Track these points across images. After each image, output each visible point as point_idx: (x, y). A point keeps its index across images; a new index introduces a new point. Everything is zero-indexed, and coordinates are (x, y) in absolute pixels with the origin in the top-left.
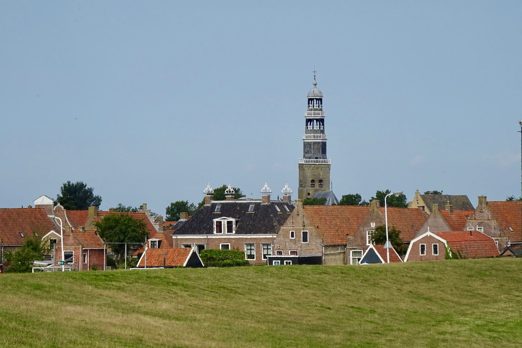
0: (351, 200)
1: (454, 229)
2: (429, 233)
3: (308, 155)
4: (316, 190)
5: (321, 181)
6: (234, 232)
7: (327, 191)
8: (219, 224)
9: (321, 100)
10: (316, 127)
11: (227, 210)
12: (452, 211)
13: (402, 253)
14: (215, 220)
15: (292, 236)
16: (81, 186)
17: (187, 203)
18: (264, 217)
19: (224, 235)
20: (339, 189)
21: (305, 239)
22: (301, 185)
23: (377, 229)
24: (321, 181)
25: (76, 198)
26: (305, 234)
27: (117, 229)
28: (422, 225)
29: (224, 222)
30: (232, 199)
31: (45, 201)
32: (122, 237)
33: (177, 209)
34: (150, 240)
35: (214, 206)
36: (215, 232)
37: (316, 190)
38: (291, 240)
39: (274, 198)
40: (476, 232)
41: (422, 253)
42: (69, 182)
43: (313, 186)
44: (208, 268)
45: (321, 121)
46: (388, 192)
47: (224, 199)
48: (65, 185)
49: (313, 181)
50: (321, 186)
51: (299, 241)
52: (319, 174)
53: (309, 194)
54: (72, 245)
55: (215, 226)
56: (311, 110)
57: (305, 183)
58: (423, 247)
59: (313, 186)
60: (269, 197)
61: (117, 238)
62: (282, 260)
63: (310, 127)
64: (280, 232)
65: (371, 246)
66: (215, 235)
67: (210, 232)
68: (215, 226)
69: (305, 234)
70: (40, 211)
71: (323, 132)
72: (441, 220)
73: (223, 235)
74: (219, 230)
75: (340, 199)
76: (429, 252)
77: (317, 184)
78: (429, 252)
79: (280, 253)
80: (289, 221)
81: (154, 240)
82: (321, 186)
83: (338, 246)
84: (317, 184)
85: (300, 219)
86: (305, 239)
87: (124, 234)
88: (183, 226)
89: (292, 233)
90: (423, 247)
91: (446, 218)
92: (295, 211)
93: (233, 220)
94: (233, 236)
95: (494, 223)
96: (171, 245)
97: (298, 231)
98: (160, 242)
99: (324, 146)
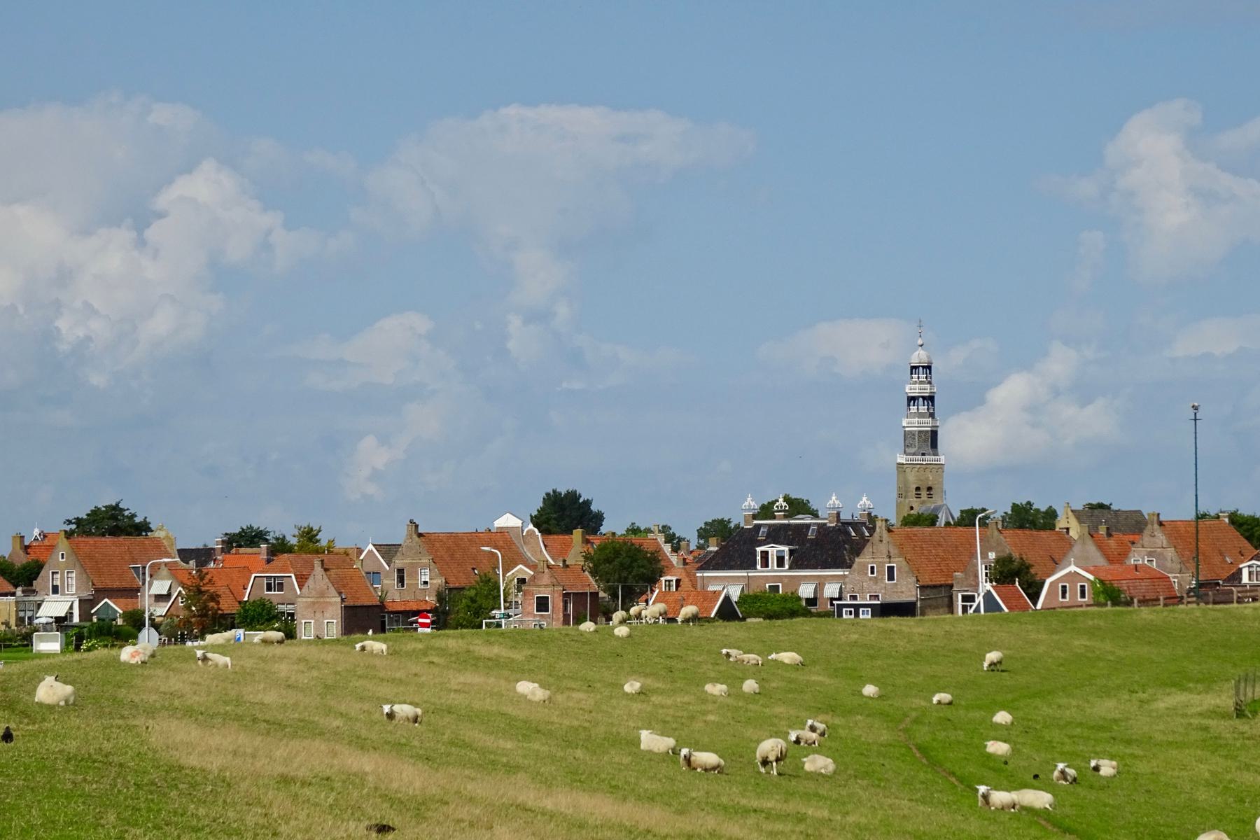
0: (968, 518)
1: (1110, 560)
2: (1073, 568)
3: (908, 450)
4: (923, 503)
5: (929, 489)
6: (787, 567)
7: (939, 503)
8: (765, 555)
9: (929, 367)
10: (923, 409)
11: (776, 535)
12: (1109, 535)
13: (1034, 598)
14: (759, 549)
15: (872, 572)
16: (573, 496)
17: (729, 522)
18: (833, 545)
19: (773, 570)
20: (953, 503)
21: (891, 578)
22: (900, 495)
23: (997, 561)
24: (929, 489)
25: (564, 514)
26: (891, 569)
27: (616, 563)
28: (1065, 555)
29: (773, 550)
30: (786, 517)
31: (508, 521)
32: (625, 574)
33: (717, 529)
34: (663, 579)
35: (758, 527)
36: (759, 567)
37: (923, 503)
38: (871, 579)
39: (845, 517)
40: (1144, 566)
41: (1064, 596)
42: (554, 491)
43: (918, 496)
44: (749, 620)
45: (930, 399)
46: (984, 510)
47: (774, 518)
48: (548, 494)
49: (918, 489)
50: (930, 496)
51: (883, 579)
52: (927, 479)
53: (912, 508)
54: (546, 586)
55: (759, 558)
56: (915, 383)
57: (907, 492)
58: (1064, 587)
59: (918, 496)
60: (838, 514)
61: (617, 576)
62: (857, 607)
63: (913, 409)
64: (855, 566)
65: (988, 586)
66: (759, 571)
67: (752, 566)
68: (759, 558)
69: (891, 569)
70: (503, 538)
71: (932, 415)
72: (1091, 548)
73: (773, 570)
74: (765, 563)
75: (957, 515)
76: (1073, 596)
77: (924, 493)
78: (1073, 596)
79: (854, 598)
80: (868, 549)
81: (669, 578)
82: (930, 496)
83: (941, 586)
84: (924, 493)
85: (883, 548)
86: (891, 578)
87: (627, 571)
88: (713, 558)
89: (872, 568)
90: (1064, 587)
91: (1100, 547)
92: (876, 535)
93: (786, 549)
94: (786, 572)
95: (1170, 553)
96: (694, 586)
97: (881, 564)
98: (678, 581)
99: (934, 434)
